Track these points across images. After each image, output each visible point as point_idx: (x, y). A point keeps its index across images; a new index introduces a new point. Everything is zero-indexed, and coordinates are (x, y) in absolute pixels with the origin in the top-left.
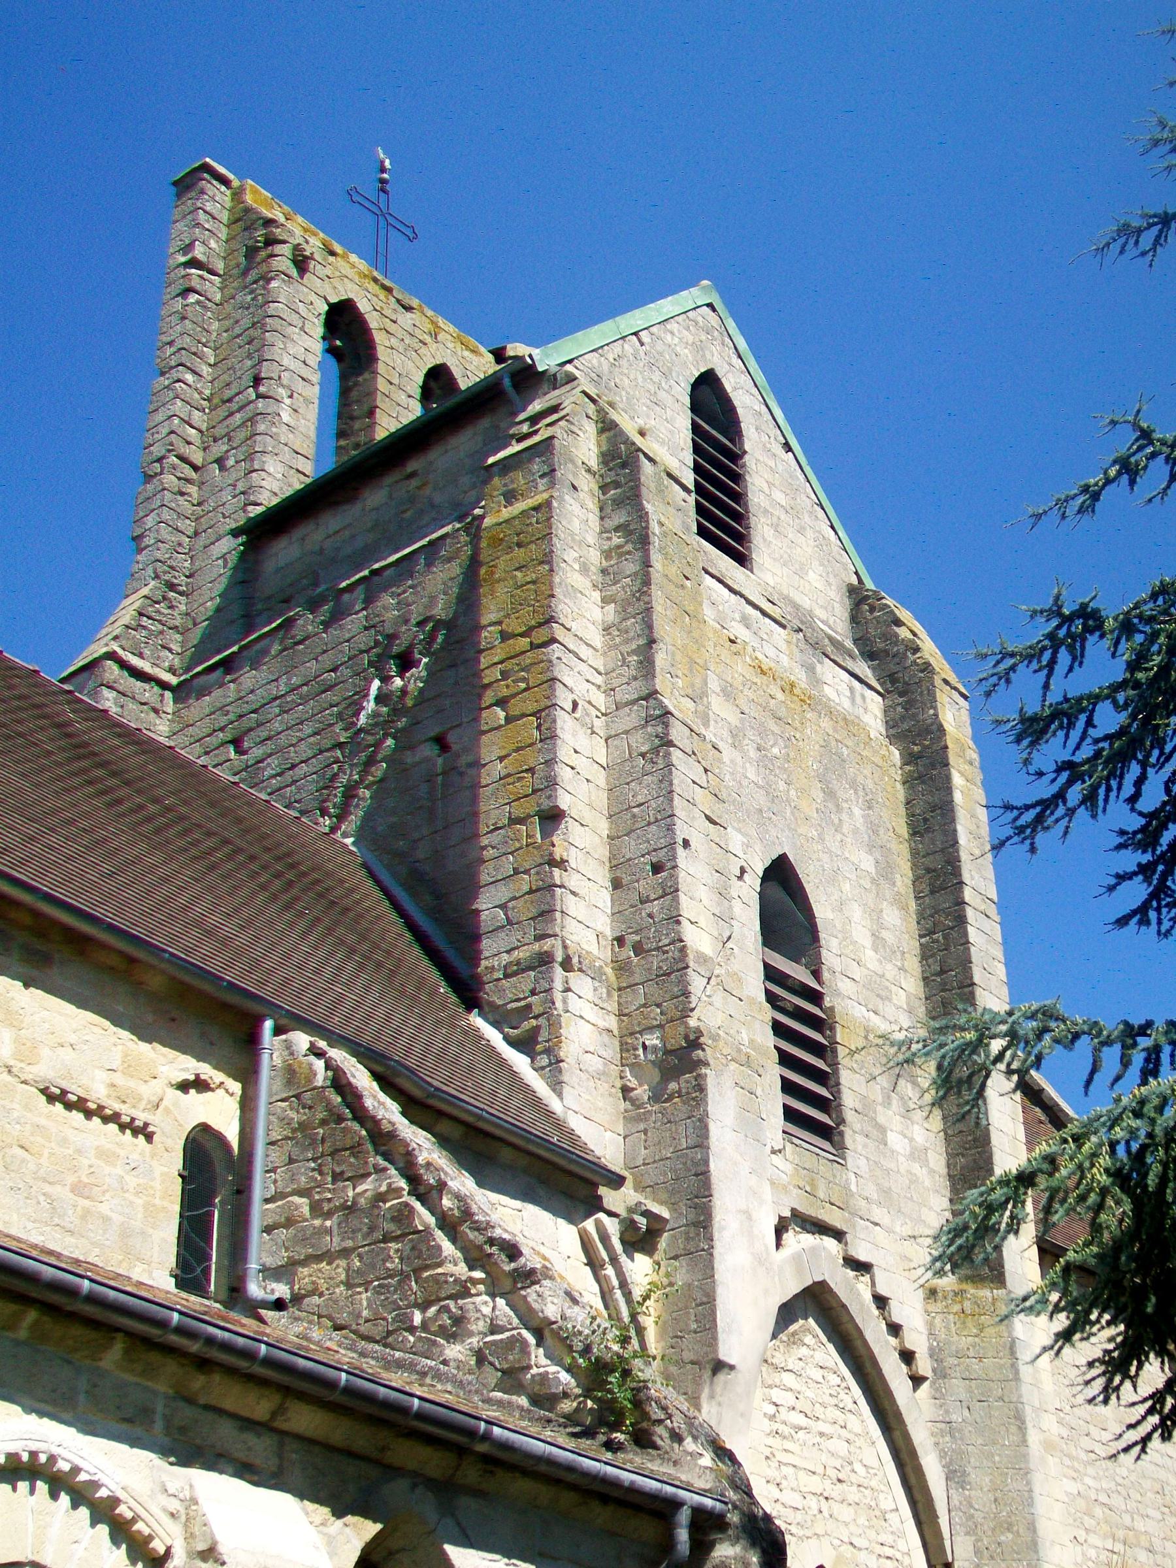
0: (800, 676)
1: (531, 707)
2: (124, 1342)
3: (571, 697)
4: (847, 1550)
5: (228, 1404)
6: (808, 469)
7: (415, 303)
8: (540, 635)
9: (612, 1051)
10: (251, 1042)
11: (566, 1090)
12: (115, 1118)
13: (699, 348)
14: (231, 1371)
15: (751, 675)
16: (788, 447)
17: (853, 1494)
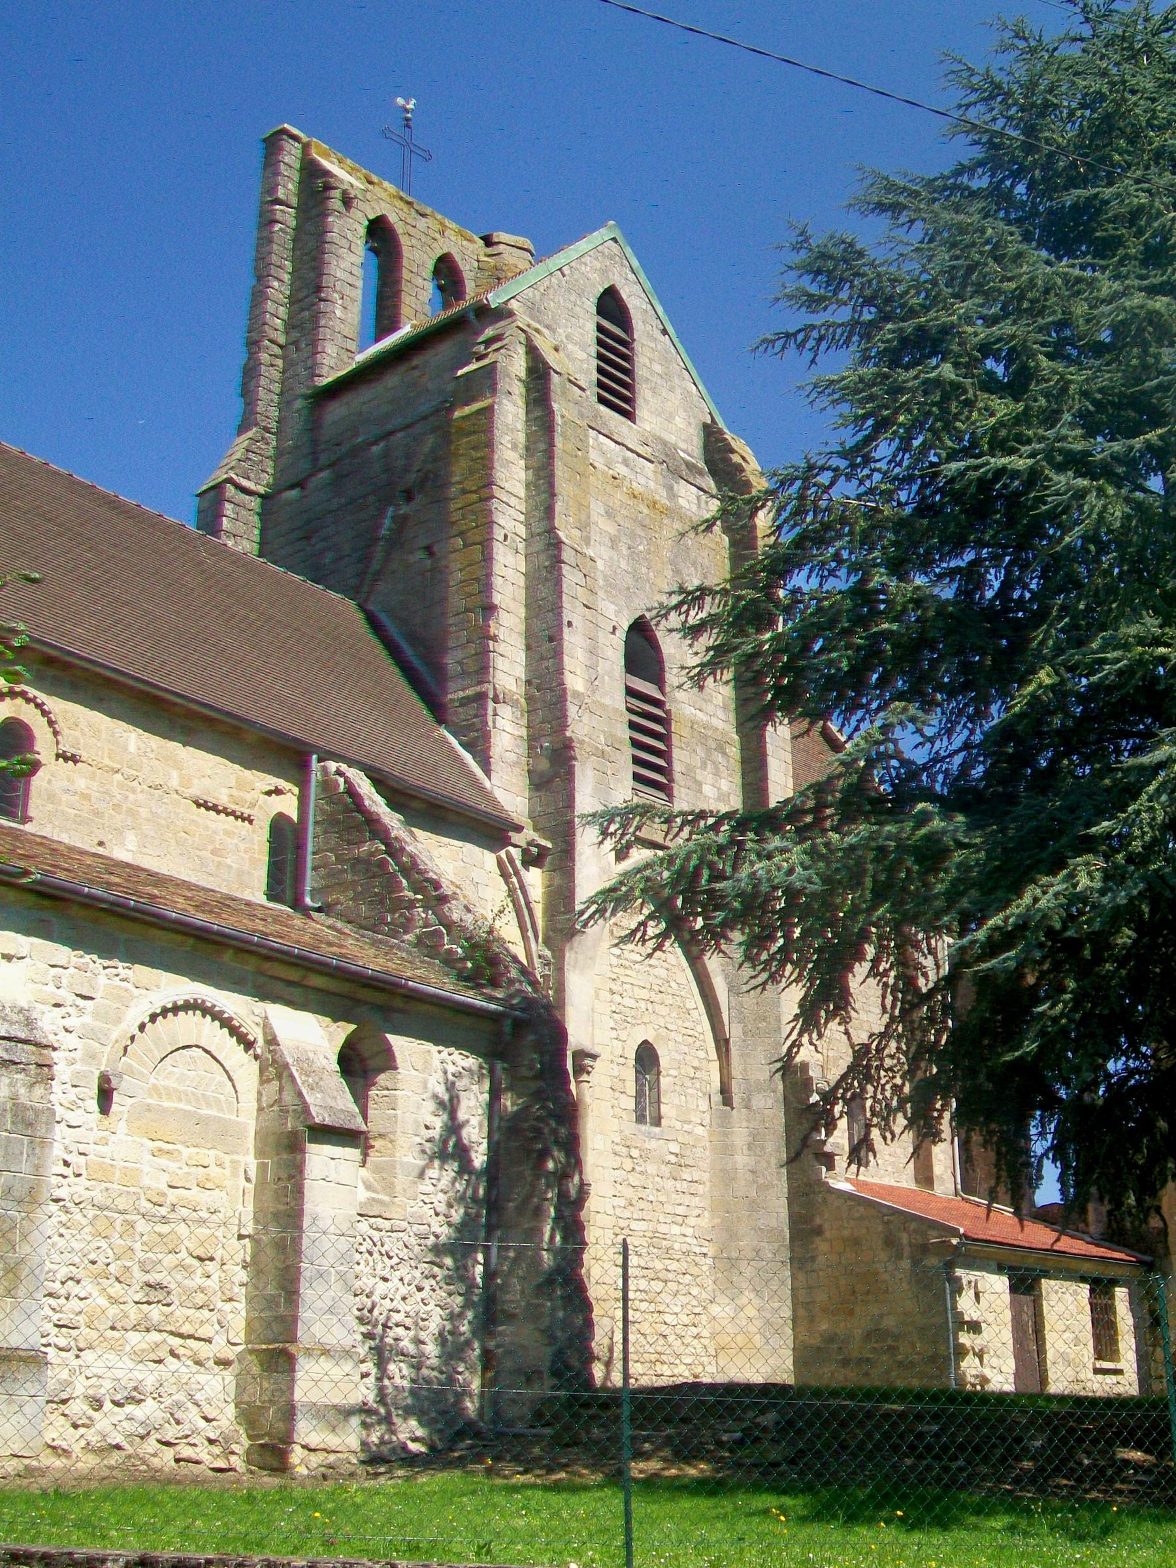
0: (662, 496)
1: (478, 539)
3: (503, 532)
4: (663, 1032)
6: (679, 346)
7: (428, 211)
8: (484, 493)
9: (523, 749)
10: (304, 766)
11: (493, 774)
12: (233, 813)
13: (604, 272)
15: (625, 499)
16: (665, 332)
17: (669, 1000)
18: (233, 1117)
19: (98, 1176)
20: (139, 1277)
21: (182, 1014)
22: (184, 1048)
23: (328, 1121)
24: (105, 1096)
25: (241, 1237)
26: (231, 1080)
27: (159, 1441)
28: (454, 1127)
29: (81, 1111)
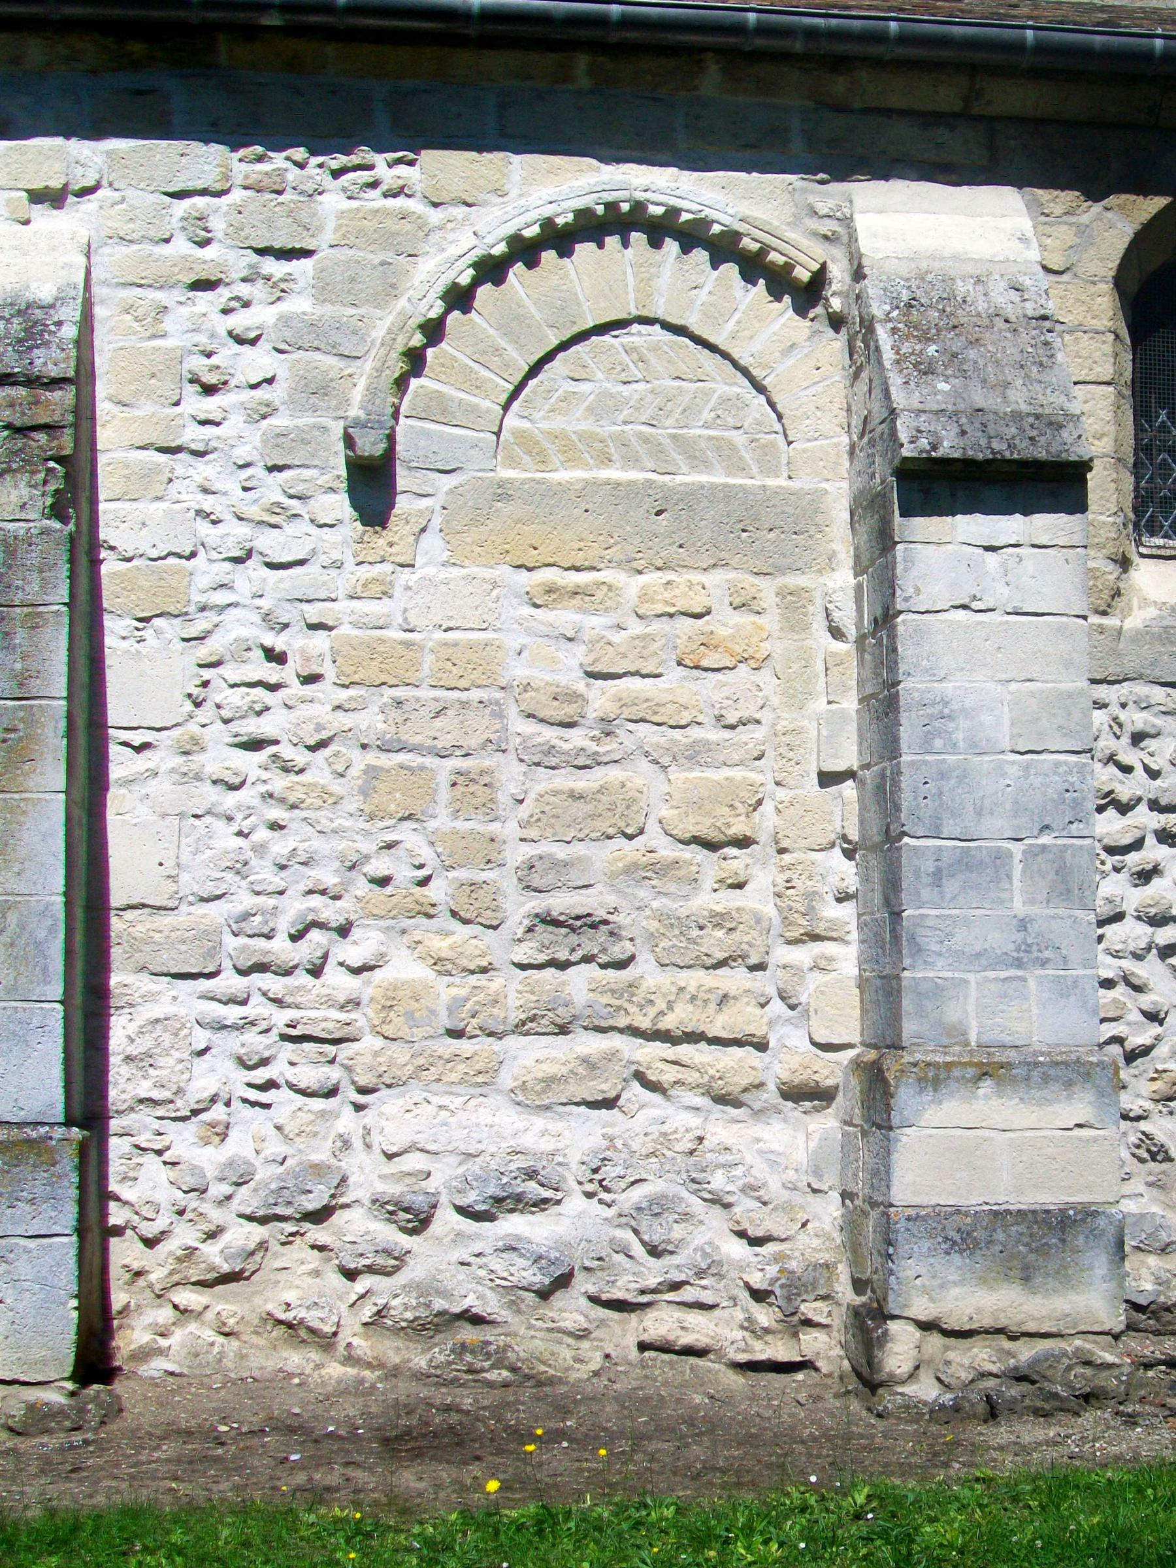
2: (718, 62)
5: (896, 100)
14: (878, 63)
18: (782, 482)
19: (372, 673)
21: (584, 250)
22: (602, 329)
23: (950, 447)
25: (827, 779)
26: (760, 388)
27: (594, 1300)
29: (303, 526)
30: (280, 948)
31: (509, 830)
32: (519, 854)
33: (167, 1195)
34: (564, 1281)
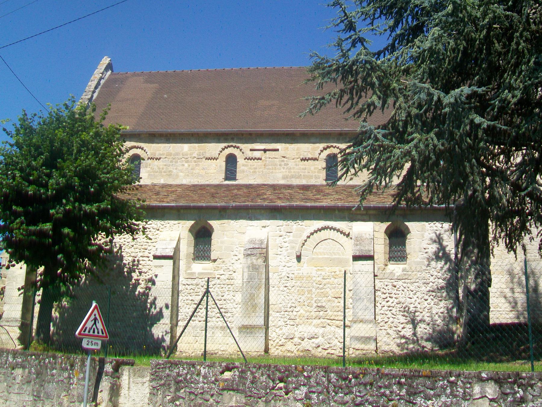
20: (315, 305)
24: (299, 258)
28: (442, 248)
30: (289, 309)
31: (313, 296)
32: (315, 299)
33: (276, 336)
34: (319, 346)
